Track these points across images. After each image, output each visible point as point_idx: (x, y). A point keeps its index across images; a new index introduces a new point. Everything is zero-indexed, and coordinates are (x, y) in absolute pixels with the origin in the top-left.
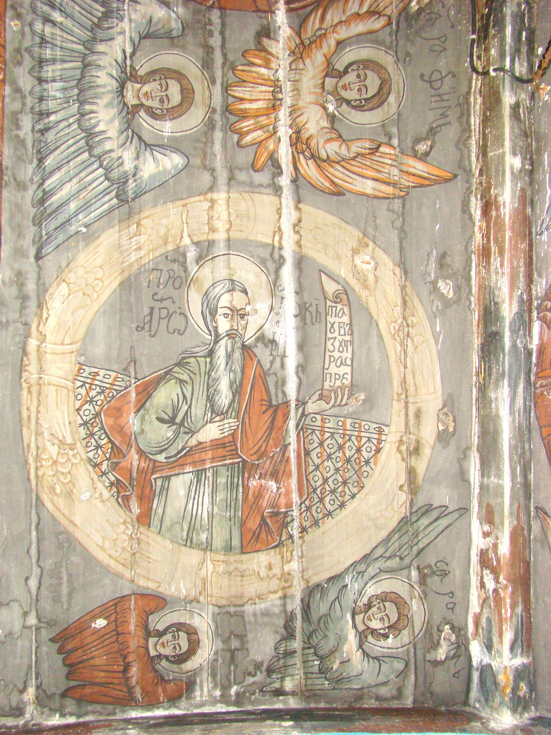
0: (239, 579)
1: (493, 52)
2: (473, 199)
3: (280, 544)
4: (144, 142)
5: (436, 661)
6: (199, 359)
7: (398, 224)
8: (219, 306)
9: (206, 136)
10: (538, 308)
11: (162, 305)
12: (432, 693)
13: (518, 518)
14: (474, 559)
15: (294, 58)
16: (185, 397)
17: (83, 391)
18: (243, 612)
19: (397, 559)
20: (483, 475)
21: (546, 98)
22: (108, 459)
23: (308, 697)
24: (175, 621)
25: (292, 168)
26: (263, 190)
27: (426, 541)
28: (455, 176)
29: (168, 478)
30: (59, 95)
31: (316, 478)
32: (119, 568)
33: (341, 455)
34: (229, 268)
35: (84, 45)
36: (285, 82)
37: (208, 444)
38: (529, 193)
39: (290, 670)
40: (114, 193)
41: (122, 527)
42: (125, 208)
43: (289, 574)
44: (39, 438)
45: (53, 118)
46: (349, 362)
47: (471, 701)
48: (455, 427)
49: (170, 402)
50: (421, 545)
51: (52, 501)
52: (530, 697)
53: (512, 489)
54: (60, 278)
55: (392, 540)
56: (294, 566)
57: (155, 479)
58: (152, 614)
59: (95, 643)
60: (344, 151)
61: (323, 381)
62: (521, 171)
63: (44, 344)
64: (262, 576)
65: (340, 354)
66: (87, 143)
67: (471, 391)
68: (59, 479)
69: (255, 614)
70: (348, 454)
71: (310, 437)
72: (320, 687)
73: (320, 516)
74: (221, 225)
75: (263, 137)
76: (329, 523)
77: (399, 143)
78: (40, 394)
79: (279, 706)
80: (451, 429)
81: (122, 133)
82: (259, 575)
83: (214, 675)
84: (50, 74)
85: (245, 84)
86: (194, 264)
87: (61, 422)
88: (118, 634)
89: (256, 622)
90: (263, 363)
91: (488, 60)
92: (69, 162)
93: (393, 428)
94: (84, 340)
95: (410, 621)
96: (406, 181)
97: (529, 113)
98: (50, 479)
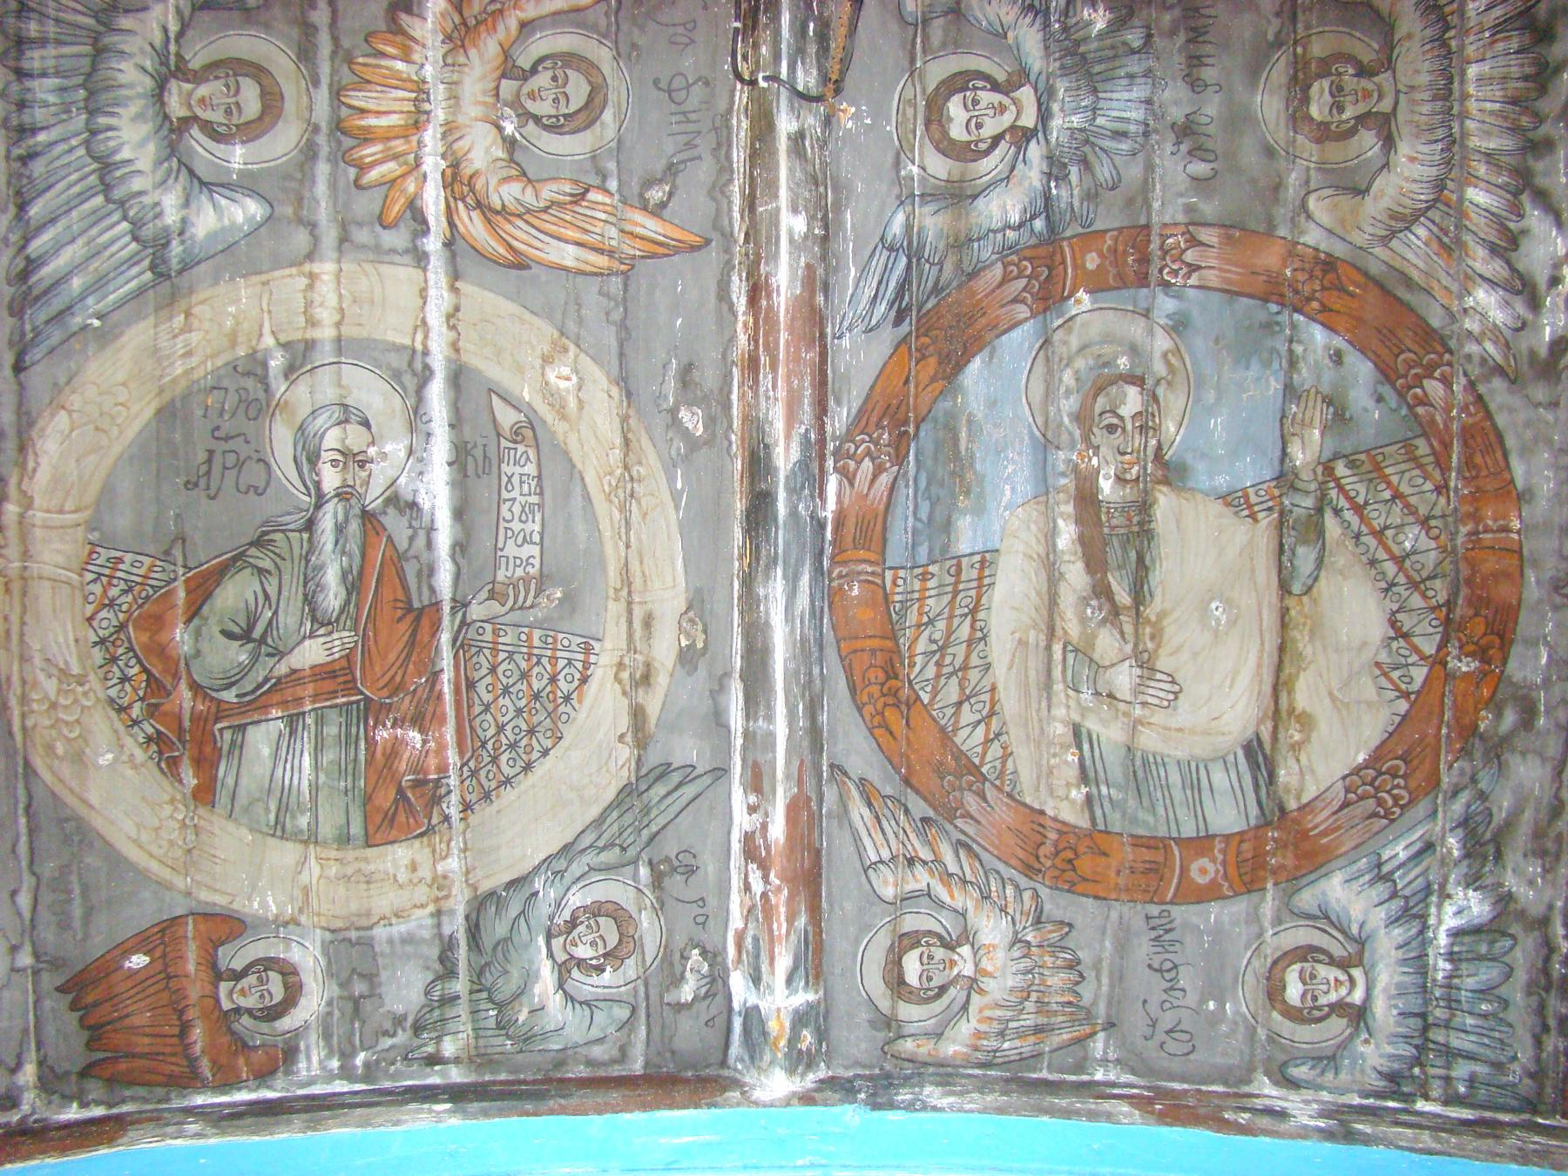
0: (364, 886)
1: (764, 50)
2: (735, 278)
3: (430, 831)
4: (199, 179)
5: (678, 1004)
6: (290, 535)
7: (617, 315)
8: (324, 447)
9: (302, 170)
10: (837, 453)
11: (227, 446)
12: (673, 1053)
13: (800, 782)
14: (736, 847)
15: (451, 46)
16: (267, 597)
17: (97, 589)
18: (372, 938)
19: (617, 849)
20: (747, 717)
21: (850, 125)
22: (142, 699)
23: (480, 1065)
24: (261, 955)
25: (445, 224)
26: (397, 259)
27: (661, 821)
28: (708, 242)
29: (242, 728)
30: (52, 99)
31: (485, 725)
32: (166, 874)
33: (524, 687)
34: (340, 385)
35: (96, 17)
36: (435, 85)
37: (308, 672)
38: (820, 271)
39: (451, 1026)
40: (146, 263)
41: (168, 809)
42: (165, 287)
43: (445, 877)
44: (27, 667)
45: (42, 137)
46: (536, 538)
47: (731, 1061)
48: (706, 642)
49: (242, 605)
50: (654, 828)
51: (50, 768)
52: (819, 1051)
53: (789, 738)
54: (56, 403)
55: (609, 821)
56: (453, 864)
57: (221, 730)
58: (222, 944)
59: (132, 992)
60: (529, 198)
61: (496, 568)
62: (806, 237)
63: (30, 512)
64: (401, 881)
65: (522, 526)
66: (102, 179)
67: (732, 584)
68: (60, 733)
69: (391, 942)
70: (536, 686)
71: (475, 659)
72: (499, 1049)
73: (493, 784)
74: (326, 315)
75: (398, 173)
76: (508, 794)
77: (619, 186)
78: (24, 594)
79: (435, 1080)
80: (700, 645)
81: (161, 163)
82: (396, 880)
83: (327, 1035)
84: (37, 64)
85: (369, 87)
86: (281, 378)
87: (61, 640)
88: (169, 978)
89: (393, 953)
90: (396, 540)
91: (758, 62)
92: (71, 210)
93: (608, 645)
94: (97, 504)
95: (638, 945)
96: (630, 248)
97: (821, 148)
98: (45, 732)
